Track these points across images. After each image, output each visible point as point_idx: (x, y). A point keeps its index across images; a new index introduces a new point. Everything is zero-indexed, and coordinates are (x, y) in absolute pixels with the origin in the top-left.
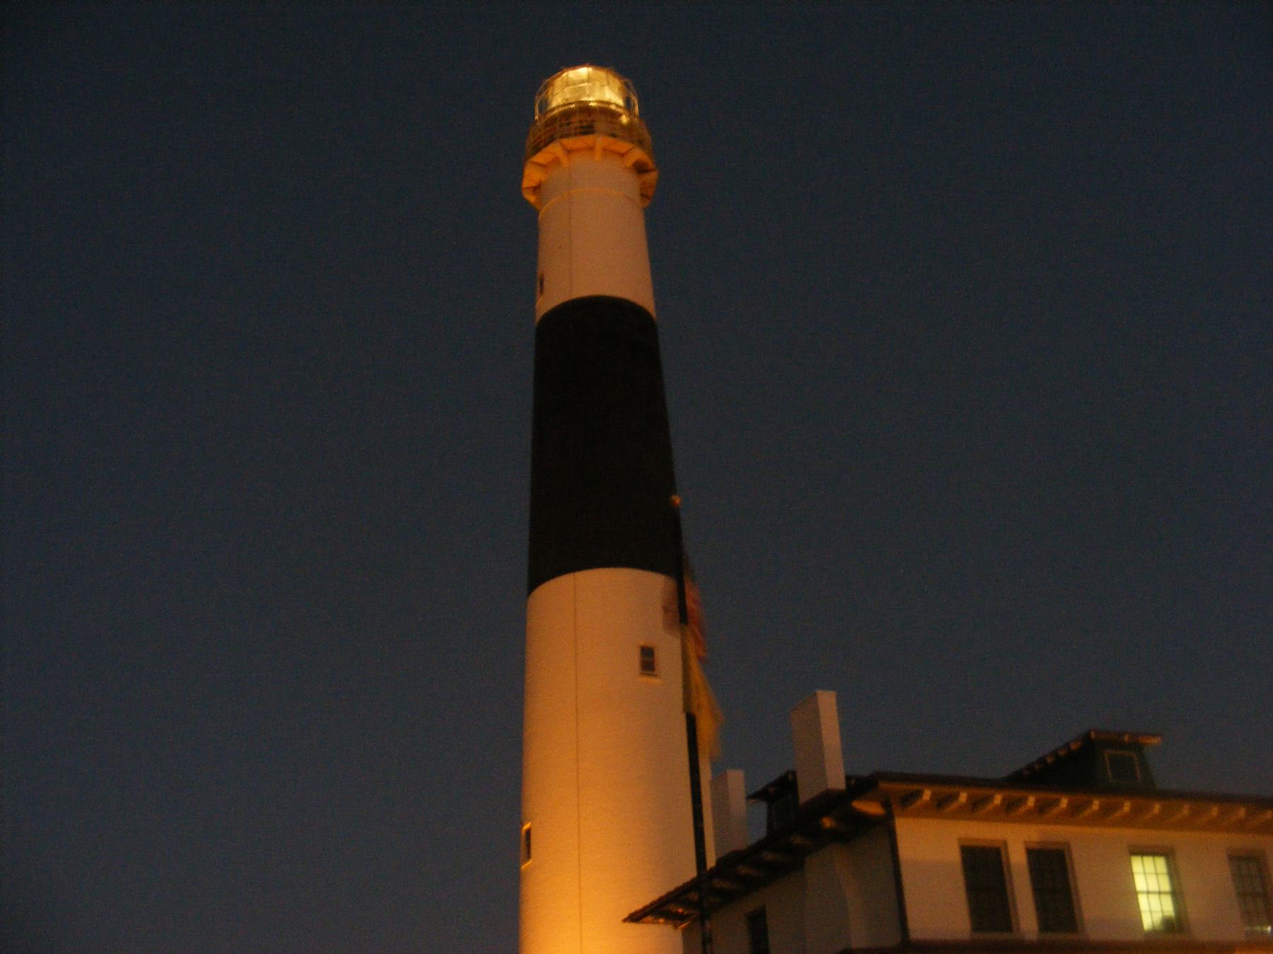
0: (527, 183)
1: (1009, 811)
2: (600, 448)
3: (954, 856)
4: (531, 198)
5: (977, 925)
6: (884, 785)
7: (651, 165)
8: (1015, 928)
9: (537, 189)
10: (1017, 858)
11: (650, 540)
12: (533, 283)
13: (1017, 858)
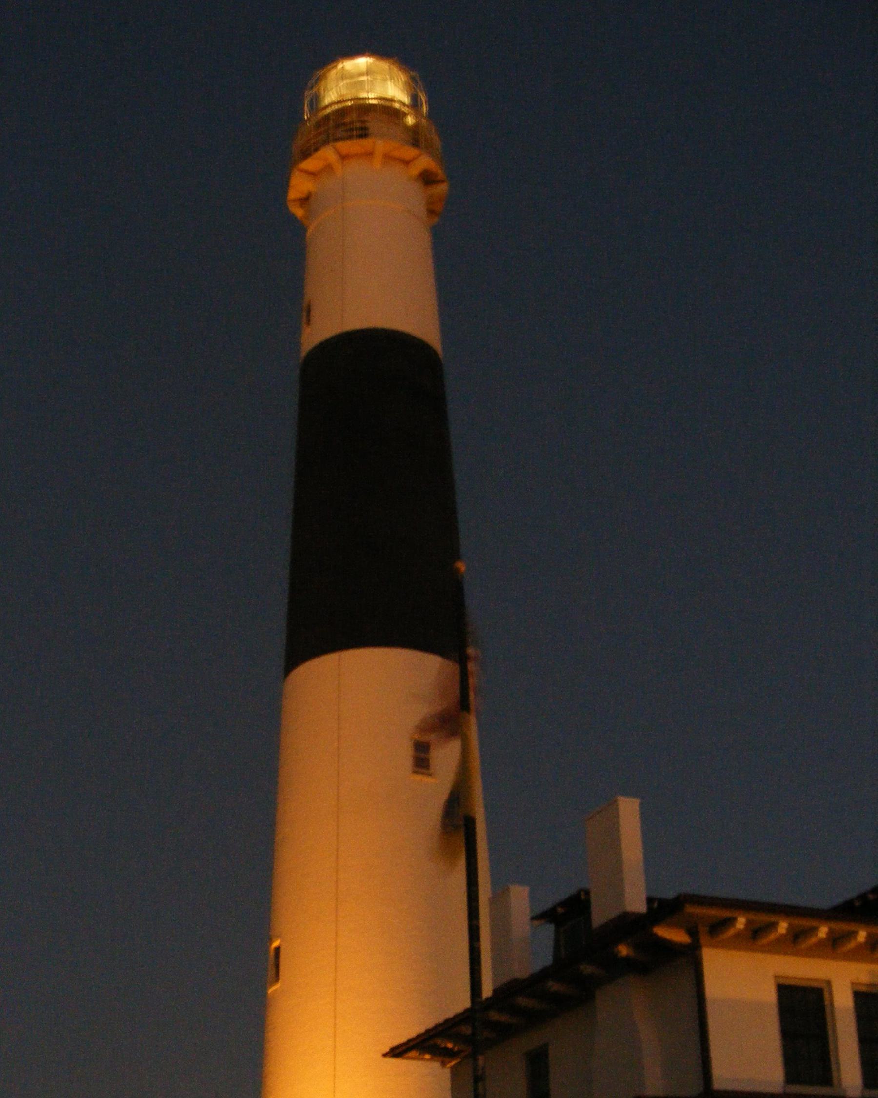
1: (834, 945)
2: (373, 504)
3: (770, 996)
4: (299, 212)
5: (791, 1077)
6: (690, 909)
7: (440, 173)
9: (305, 201)
10: (842, 1001)
11: (430, 619)
12: (295, 305)
13: (842, 1001)
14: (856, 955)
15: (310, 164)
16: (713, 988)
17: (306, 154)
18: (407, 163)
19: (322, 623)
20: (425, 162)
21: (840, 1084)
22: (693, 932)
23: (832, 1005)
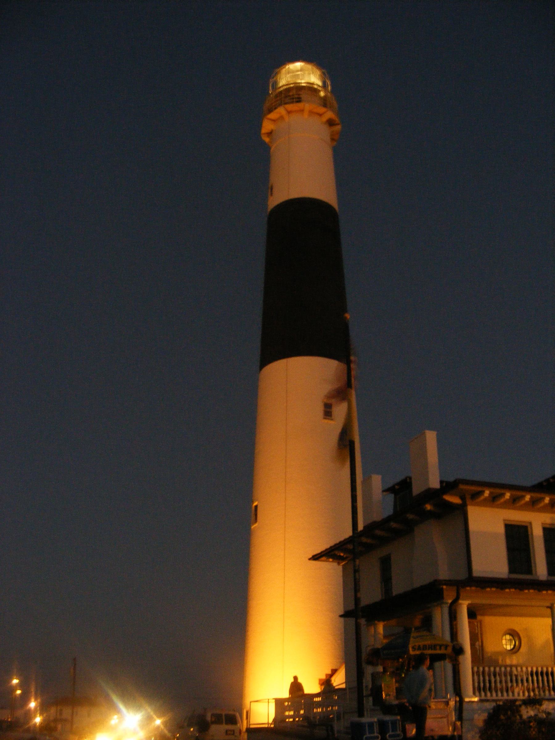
0: (264, 131)
1: (533, 505)
2: (303, 285)
3: (501, 530)
4: (267, 139)
6: (462, 487)
7: (337, 120)
8: (534, 572)
9: (270, 134)
10: (537, 532)
11: (332, 342)
13: (537, 532)
14: (544, 509)
15: (272, 116)
16: (473, 526)
17: (270, 111)
18: (320, 115)
19: (279, 344)
20: (329, 115)
21: (536, 574)
22: (463, 498)
23: (532, 534)
